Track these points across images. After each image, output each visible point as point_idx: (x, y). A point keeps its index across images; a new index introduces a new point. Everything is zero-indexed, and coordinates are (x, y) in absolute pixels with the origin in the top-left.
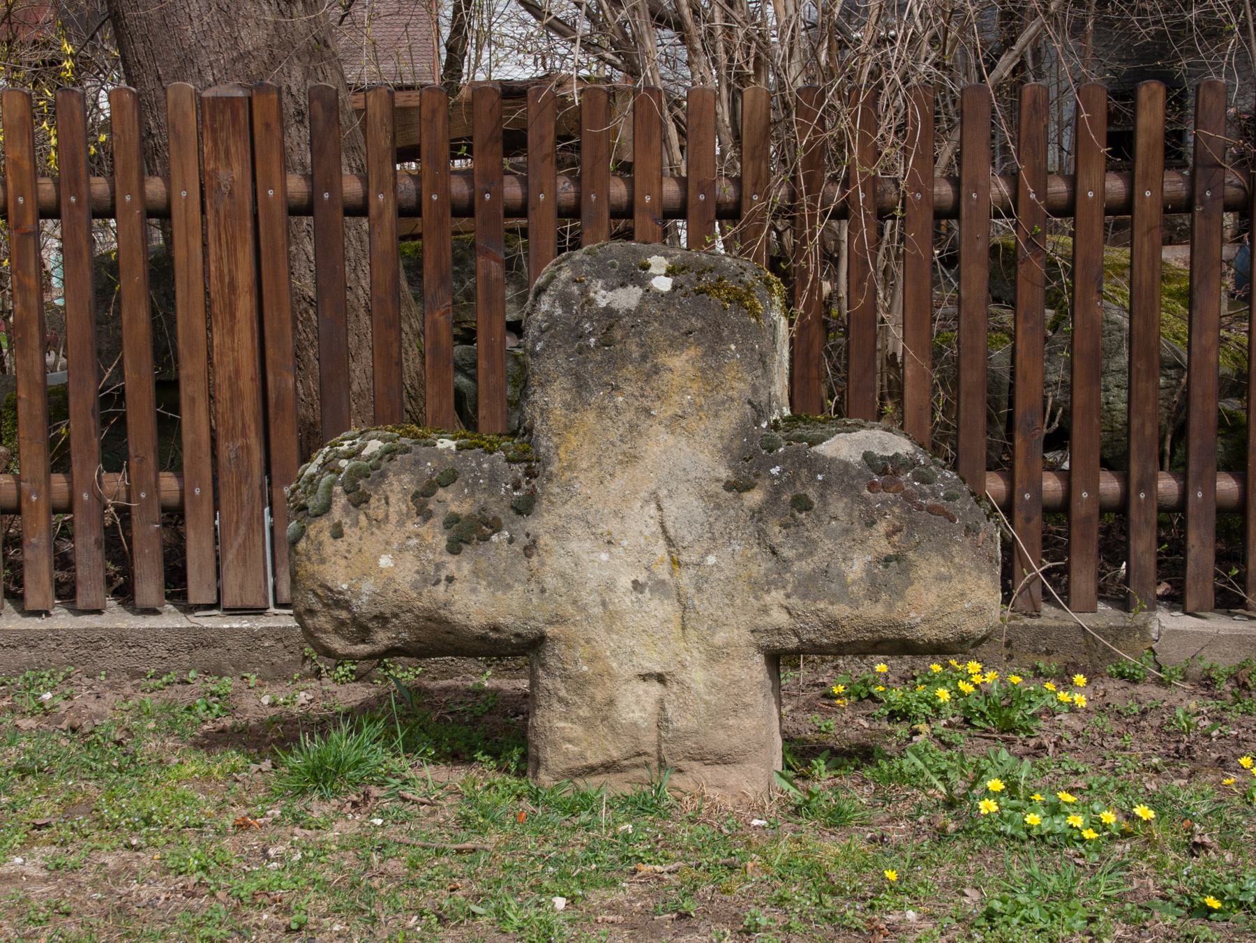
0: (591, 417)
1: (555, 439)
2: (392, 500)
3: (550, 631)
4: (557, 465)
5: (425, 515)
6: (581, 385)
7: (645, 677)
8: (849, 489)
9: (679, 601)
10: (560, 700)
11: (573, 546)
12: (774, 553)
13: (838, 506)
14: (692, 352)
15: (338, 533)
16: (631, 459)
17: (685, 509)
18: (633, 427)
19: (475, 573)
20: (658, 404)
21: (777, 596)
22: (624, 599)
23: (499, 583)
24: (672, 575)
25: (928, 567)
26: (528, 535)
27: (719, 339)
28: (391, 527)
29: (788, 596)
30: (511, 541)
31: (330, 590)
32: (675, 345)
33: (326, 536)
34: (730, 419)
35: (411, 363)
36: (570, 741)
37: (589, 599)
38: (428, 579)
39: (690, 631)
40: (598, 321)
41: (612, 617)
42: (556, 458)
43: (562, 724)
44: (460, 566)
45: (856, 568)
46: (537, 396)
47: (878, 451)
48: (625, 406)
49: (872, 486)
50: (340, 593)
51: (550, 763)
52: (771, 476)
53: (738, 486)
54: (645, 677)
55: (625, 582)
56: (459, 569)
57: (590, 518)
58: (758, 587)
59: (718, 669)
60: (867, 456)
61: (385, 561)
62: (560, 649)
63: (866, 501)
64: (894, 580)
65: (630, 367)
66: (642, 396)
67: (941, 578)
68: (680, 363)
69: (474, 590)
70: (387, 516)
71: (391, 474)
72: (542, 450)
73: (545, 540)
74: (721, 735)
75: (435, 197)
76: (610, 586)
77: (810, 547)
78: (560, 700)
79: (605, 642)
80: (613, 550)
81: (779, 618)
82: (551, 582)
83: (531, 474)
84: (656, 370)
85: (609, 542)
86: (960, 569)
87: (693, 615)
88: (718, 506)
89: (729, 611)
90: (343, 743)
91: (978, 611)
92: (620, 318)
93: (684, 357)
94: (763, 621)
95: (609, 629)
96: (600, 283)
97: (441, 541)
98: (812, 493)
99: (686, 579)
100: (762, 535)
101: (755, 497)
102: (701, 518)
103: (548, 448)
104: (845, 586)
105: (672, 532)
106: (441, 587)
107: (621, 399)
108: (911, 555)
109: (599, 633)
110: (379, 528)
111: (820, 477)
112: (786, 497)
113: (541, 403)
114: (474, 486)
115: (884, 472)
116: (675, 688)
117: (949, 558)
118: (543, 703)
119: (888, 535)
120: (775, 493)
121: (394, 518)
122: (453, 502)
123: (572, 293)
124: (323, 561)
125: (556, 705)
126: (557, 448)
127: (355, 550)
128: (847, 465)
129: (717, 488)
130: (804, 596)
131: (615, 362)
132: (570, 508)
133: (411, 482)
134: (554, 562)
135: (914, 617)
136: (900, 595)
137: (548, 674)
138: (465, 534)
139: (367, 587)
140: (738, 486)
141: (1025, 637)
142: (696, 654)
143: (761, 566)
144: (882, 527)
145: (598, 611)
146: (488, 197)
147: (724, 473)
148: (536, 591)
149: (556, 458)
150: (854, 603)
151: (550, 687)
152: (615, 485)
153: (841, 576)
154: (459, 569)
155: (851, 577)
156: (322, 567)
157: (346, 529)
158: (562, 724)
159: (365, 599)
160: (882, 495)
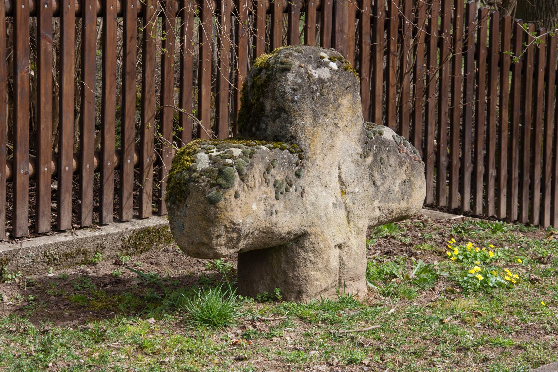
1: (308, 141)
2: (256, 177)
3: (309, 230)
4: (310, 153)
5: (267, 182)
9: (346, 210)
10: (311, 262)
11: (315, 190)
12: (374, 184)
15: (236, 196)
17: (348, 168)
18: (331, 133)
19: (285, 207)
20: (340, 121)
23: (293, 211)
24: (342, 198)
26: (301, 187)
28: (256, 190)
29: (380, 202)
30: (296, 190)
31: (234, 224)
32: (344, 94)
33: (232, 198)
36: (317, 280)
39: (352, 223)
40: (318, 84)
42: (309, 150)
43: (312, 273)
44: (279, 205)
46: (298, 121)
48: (329, 123)
50: (239, 225)
51: (309, 292)
53: (365, 155)
56: (279, 206)
57: (321, 176)
62: (312, 238)
64: (408, 190)
65: (331, 105)
66: (335, 118)
69: (285, 216)
70: (254, 185)
71: (255, 164)
72: (303, 147)
75: (23, 6)
78: (311, 262)
80: (327, 190)
82: (309, 208)
83: (301, 158)
85: (326, 186)
87: (352, 215)
88: (358, 165)
89: (363, 211)
90: (212, 298)
92: (326, 83)
93: (346, 99)
96: (311, 66)
99: (348, 198)
102: (354, 171)
103: (305, 145)
105: (344, 179)
106: (274, 216)
107: (327, 120)
110: (252, 190)
111: (388, 149)
113: (301, 124)
114: (283, 166)
116: (346, 249)
118: (301, 265)
121: (257, 185)
123: (302, 72)
124: (232, 210)
125: (309, 265)
126: (310, 145)
127: (244, 202)
129: (357, 157)
130: (385, 201)
133: (262, 167)
134: (309, 198)
137: (304, 251)
138: (281, 190)
139: (249, 220)
140: (365, 155)
142: (353, 233)
146: (46, 6)
148: (305, 213)
149: (309, 150)
151: (306, 256)
152: (328, 160)
154: (279, 206)
156: (232, 213)
157: (240, 192)
158: (312, 273)
159: (247, 226)
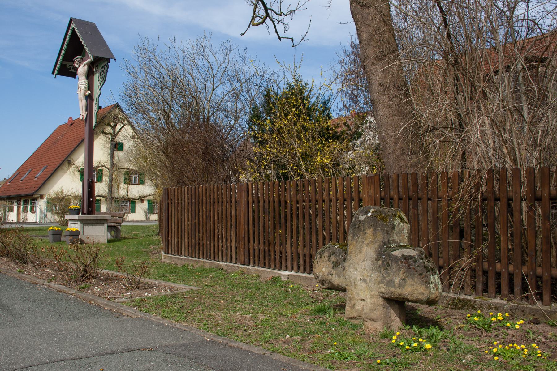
0: (355, 242)
3: (346, 287)
6: (354, 236)
7: (361, 300)
8: (396, 262)
13: (394, 266)
14: (371, 230)
16: (360, 252)
21: (383, 285)
22: (358, 282)
25: (409, 282)
27: (377, 227)
32: (369, 228)
34: (377, 245)
35: (401, 193)
37: (352, 281)
38: (329, 274)
41: (356, 286)
45: (397, 280)
47: (405, 254)
49: (402, 262)
52: (384, 258)
54: (361, 300)
55: (358, 278)
58: (380, 282)
59: (373, 300)
60: (403, 255)
61: (323, 269)
63: (399, 265)
67: (412, 285)
68: (369, 232)
73: (347, 268)
74: (373, 315)
76: (356, 279)
77: (389, 274)
79: (354, 291)
81: (383, 290)
82: (347, 277)
84: (365, 233)
86: (416, 283)
91: (421, 294)
94: (380, 290)
95: (355, 288)
97: (331, 266)
98: (390, 262)
100: (380, 271)
101: (380, 262)
104: (394, 284)
108: (407, 279)
109: (353, 289)
112: (385, 263)
115: (405, 259)
117: (414, 280)
119: (403, 274)
120: (383, 262)
122: (333, 258)
128: (397, 256)
129: (374, 260)
130: (387, 286)
131: (359, 231)
132: (350, 262)
135: (407, 293)
136: (404, 287)
140: (377, 260)
141: (527, 310)
143: (380, 278)
144: (401, 272)
145: (353, 284)
147: (375, 256)
150: (395, 288)
152: (358, 257)
153: (394, 282)
155: (396, 282)
160: (404, 264)
